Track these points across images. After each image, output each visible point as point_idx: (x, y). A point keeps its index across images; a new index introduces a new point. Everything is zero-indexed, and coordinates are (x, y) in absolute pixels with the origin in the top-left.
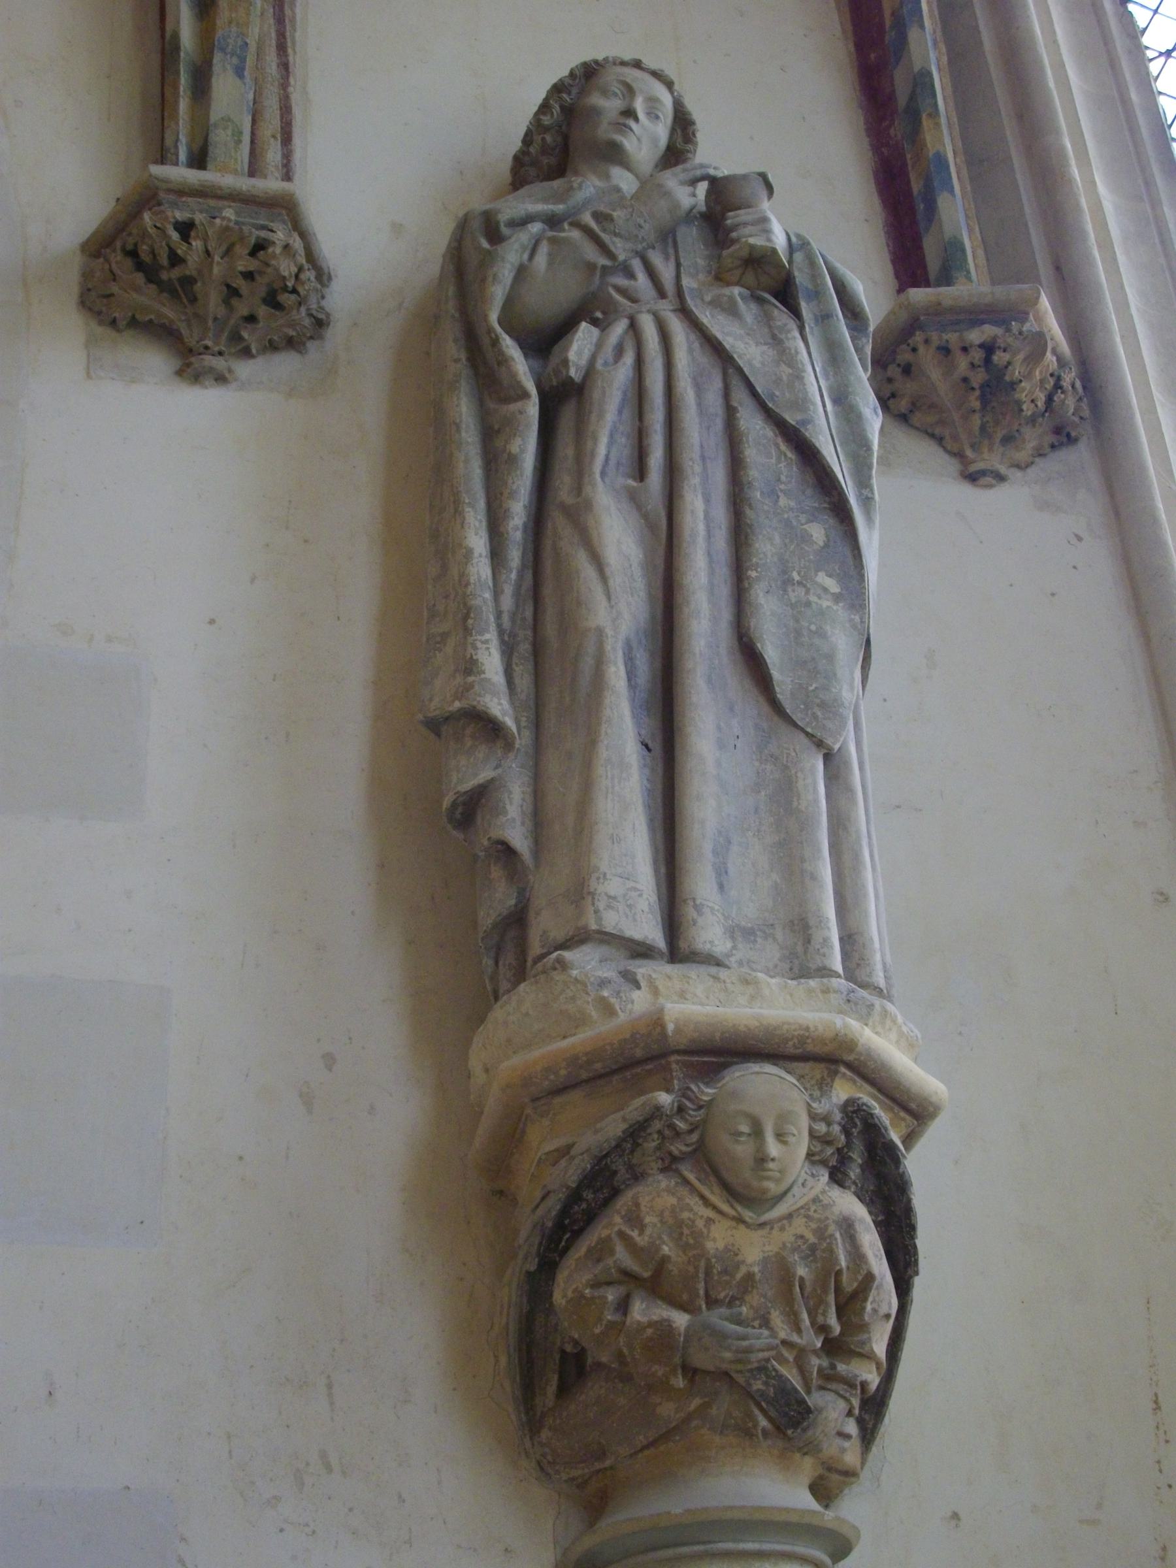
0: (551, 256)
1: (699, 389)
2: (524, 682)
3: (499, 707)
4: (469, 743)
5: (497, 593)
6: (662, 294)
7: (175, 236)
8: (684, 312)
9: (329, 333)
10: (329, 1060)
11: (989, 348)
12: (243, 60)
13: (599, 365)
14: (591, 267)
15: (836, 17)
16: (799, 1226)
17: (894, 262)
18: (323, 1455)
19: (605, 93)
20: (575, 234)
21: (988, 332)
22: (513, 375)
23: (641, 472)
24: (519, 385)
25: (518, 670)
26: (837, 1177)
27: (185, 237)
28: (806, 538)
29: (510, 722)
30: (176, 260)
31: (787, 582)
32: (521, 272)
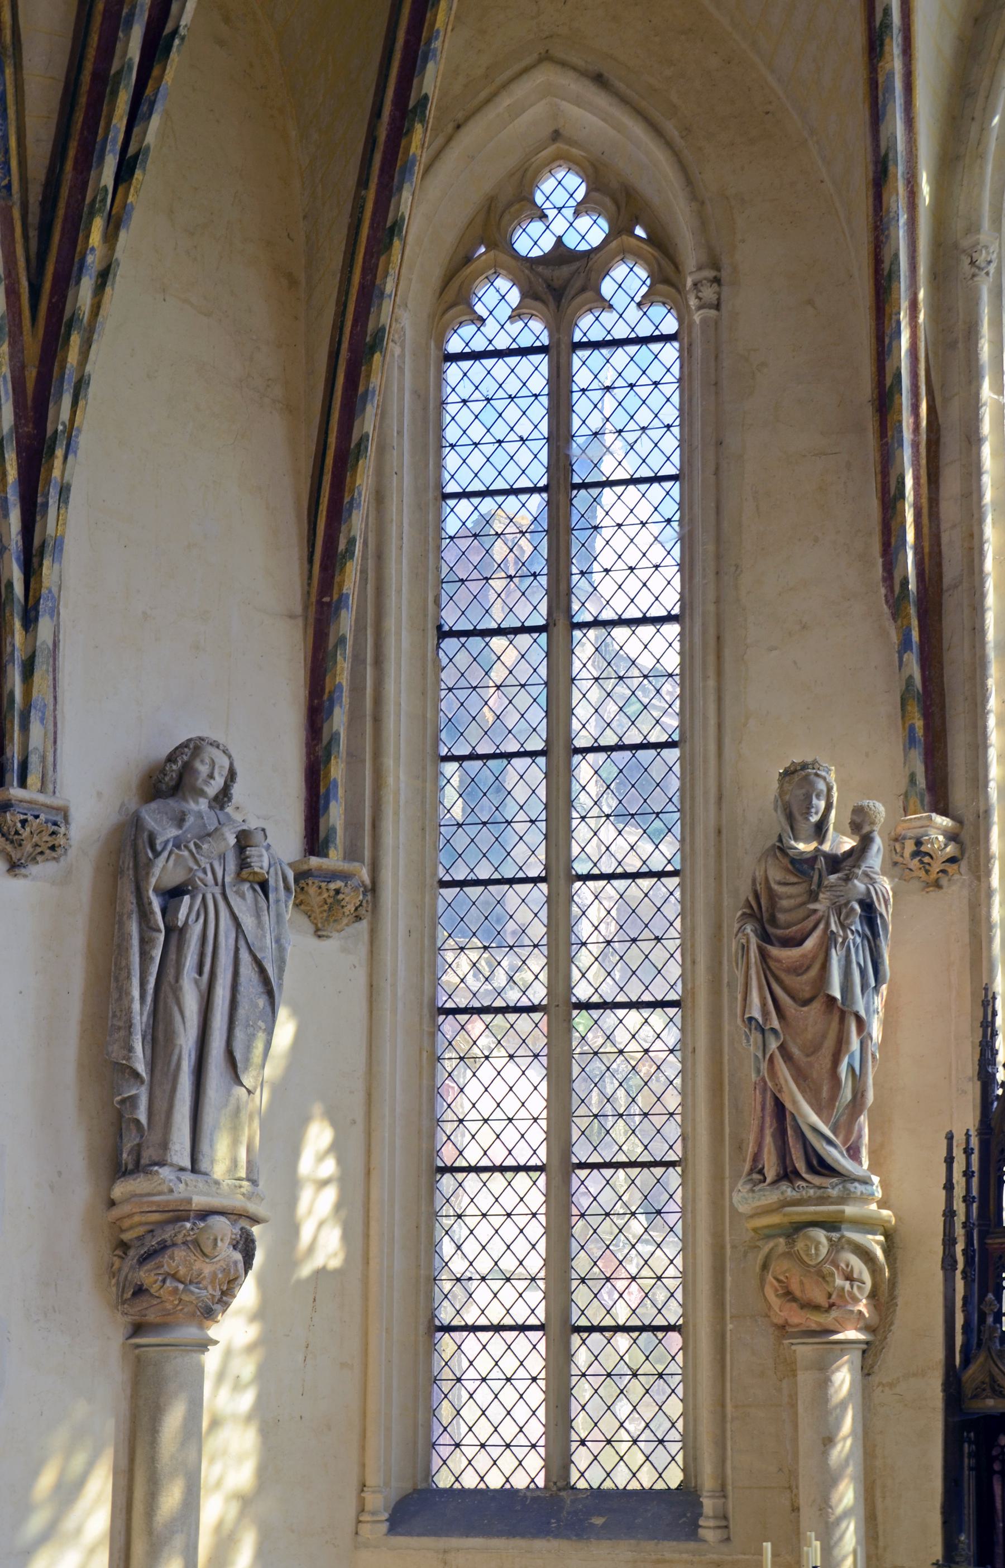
0: (176, 861)
1: (227, 938)
2: (149, 1052)
3: (141, 1068)
4: (127, 1076)
5: (141, 1014)
6: (216, 884)
7: (19, 825)
8: (224, 895)
9: (69, 852)
10: (60, 1173)
11: (337, 892)
12: (44, 713)
13: (190, 922)
14: (191, 870)
15: (303, 672)
16: (222, 1263)
17: (306, 821)
18: (53, 1307)
19: (202, 761)
20: (186, 853)
21: (339, 884)
22: (156, 921)
23: (200, 973)
24: (158, 925)
25: (146, 1047)
26: (235, 1247)
27: (23, 827)
28: (257, 1006)
29: (144, 1074)
30: (17, 833)
31: (248, 1025)
32: (164, 867)
